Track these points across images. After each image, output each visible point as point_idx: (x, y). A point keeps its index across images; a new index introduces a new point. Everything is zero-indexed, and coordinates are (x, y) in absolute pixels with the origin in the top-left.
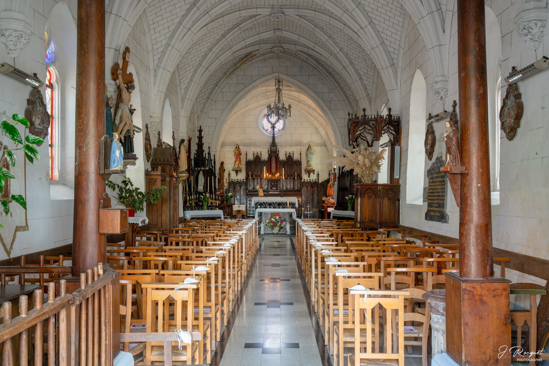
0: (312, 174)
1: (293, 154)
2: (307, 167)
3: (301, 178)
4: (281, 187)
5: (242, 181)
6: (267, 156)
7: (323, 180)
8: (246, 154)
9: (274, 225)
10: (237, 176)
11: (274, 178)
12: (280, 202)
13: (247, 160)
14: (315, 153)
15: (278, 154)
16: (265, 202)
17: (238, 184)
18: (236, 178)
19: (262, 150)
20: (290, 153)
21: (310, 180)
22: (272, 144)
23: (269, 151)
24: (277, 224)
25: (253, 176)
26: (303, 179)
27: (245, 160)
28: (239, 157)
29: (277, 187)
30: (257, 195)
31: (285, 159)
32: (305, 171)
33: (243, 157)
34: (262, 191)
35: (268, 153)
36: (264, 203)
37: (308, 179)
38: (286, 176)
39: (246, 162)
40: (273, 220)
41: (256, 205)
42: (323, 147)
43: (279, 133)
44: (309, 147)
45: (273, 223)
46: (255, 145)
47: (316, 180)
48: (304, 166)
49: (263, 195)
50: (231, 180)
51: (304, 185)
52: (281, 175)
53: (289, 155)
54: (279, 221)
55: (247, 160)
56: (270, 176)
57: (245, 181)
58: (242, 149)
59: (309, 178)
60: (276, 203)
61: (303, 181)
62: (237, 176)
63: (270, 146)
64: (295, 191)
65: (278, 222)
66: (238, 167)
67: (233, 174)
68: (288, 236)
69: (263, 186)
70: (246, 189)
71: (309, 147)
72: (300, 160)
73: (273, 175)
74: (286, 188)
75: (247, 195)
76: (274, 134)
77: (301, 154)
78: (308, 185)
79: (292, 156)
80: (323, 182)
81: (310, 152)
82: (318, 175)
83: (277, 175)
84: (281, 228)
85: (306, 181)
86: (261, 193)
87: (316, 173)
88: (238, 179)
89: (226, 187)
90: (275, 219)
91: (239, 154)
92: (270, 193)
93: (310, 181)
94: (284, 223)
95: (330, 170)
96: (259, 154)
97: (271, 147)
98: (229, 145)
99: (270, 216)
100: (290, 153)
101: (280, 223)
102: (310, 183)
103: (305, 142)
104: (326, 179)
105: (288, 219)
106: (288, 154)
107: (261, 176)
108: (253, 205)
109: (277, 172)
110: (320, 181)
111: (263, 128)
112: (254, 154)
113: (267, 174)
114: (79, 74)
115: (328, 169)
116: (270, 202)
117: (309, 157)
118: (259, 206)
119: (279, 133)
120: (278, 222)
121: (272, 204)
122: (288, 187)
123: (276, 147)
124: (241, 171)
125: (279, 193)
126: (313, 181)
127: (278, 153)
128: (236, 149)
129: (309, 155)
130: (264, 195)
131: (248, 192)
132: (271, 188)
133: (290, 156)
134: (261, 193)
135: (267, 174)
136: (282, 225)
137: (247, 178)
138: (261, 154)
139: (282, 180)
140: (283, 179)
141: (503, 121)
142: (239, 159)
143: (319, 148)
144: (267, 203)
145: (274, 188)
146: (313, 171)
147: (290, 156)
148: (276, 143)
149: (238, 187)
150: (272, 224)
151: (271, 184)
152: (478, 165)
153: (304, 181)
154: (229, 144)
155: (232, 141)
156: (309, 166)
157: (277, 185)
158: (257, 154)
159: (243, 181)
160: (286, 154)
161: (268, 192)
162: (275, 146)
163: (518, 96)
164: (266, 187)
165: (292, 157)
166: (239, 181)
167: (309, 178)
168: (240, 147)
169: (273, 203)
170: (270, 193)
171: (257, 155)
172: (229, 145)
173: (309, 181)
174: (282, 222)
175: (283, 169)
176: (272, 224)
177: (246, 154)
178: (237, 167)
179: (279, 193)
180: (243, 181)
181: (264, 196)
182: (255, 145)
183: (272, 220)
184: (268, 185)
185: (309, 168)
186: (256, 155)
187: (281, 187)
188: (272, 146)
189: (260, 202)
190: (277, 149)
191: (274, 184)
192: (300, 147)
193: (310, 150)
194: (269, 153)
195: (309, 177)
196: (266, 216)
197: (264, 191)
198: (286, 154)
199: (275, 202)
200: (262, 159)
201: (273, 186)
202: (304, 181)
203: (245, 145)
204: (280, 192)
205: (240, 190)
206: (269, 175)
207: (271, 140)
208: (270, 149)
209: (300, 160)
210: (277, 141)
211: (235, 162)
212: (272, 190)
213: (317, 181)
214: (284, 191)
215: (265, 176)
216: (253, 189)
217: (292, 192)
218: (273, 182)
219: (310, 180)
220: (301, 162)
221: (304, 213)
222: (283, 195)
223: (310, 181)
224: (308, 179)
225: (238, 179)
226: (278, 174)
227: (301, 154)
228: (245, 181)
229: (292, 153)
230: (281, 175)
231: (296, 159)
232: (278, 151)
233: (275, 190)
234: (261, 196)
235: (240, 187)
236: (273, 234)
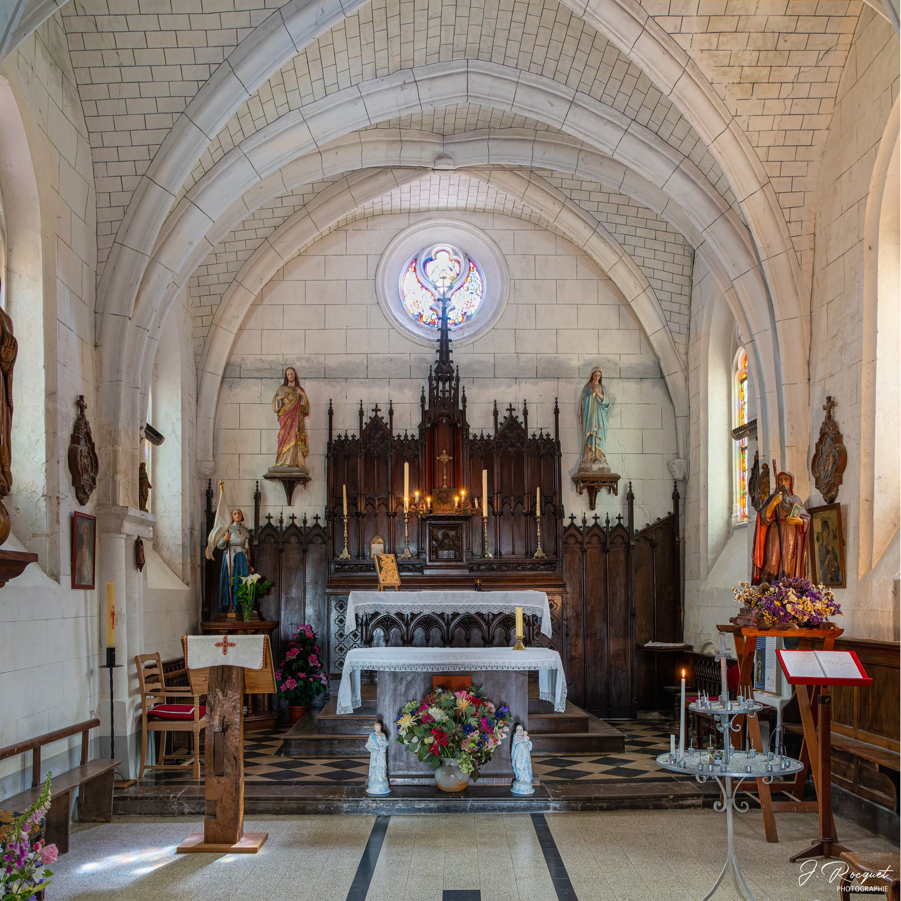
0: (603, 495)
1: (526, 413)
2: (588, 465)
3: (558, 512)
4: (477, 550)
5: (310, 523)
6: (417, 419)
7: (652, 521)
8: (331, 413)
9: (444, 744)
10: (290, 503)
11: (443, 510)
12: (473, 612)
13: (335, 438)
14: (616, 410)
15: (463, 413)
16: (407, 612)
17: (293, 540)
18: (288, 511)
19: (396, 397)
20: (511, 410)
21: (596, 518)
22: (436, 371)
23: (423, 399)
24: (459, 743)
25: (355, 505)
26: (567, 514)
27: (325, 439)
28: (296, 424)
29: (456, 547)
30: (372, 584)
31: (492, 433)
32: (576, 480)
33: (315, 424)
34: (394, 565)
35: (423, 406)
36: (400, 615)
37: (590, 514)
38: (497, 502)
39: (329, 444)
40: (436, 713)
41: (367, 624)
42: (647, 384)
43: (468, 326)
44: (594, 380)
45: (440, 735)
46: (368, 376)
47: (619, 518)
48: (570, 463)
49: (398, 583)
50: (263, 522)
51: (572, 541)
52: (475, 494)
53: (507, 414)
54: (473, 722)
55: (335, 438)
56: (429, 500)
57: (322, 523)
58: (309, 387)
59: (593, 513)
60: (455, 615)
61: (566, 522)
62: (290, 503)
63: (430, 379)
64: (535, 566)
65: (468, 729)
66: (295, 463)
67: (274, 494)
68: (523, 804)
69: (401, 545)
70: (330, 556)
71: (594, 380)
72: (552, 436)
73: (443, 498)
74: (497, 553)
75: (331, 583)
76: (444, 331)
77: (557, 412)
78: (587, 539)
79: (521, 419)
80: (649, 529)
81: (599, 402)
82: (630, 497)
83: (457, 499)
84: (481, 757)
85: (578, 523)
86: (389, 573)
87: (621, 485)
88: (293, 517)
89: (239, 550)
90: (450, 708)
91: (295, 409)
92: (427, 572)
93: (596, 525)
94: (501, 734)
95: (679, 476)
96: (384, 414)
97: (434, 382)
98: (259, 375)
99: (418, 690)
100: (511, 410)
101: (476, 736)
102: (596, 531)
103: (575, 362)
104: (663, 515)
105: (518, 707)
106: (503, 413)
107: (393, 505)
108: (350, 625)
109: (455, 486)
110: (639, 524)
111: (404, 312)
112: (361, 413)
113: (417, 494)
114: (895, 886)
115: (672, 473)
116: (427, 612)
117: (594, 422)
118: (379, 632)
119: (468, 326)
120: (468, 729)
121: (436, 622)
122: (506, 549)
123: (453, 383)
124: (305, 480)
125: (466, 572)
126: (608, 521)
127: (461, 407)
128: (287, 389)
129: (596, 415)
130: (402, 581)
131: (337, 570)
132: (434, 551)
133: (512, 421)
134: (389, 573)
135: (417, 494)
136: (491, 746)
137: (333, 512)
138: (391, 413)
139: (477, 520)
140: (485, 514)
141: (753, 495)
142: (295, 431)
143: (631, 387)
144: (414, 616)
145: (444, 554)
146: (611, 482)
147: (512, 421)
148: (454, 366)
149: (292, 555)
150: (429, 740)
151: (433, 537)
152: (846, 532)
153: (572, 524)
154: (258, 370)
155: (270, 358)
156: (595, 460)
157: (459, 538)
158: (376, 410)
159: (317, 526)
160: (496, 413)
161: (421, 570)
162: (450, 379)
163: (838, 438)
164: (413, 548)
165: (519, 425)
166: (299, 523)
167: (593, 513)
168: (307, 385)
169: (442, 615)
170: (427, 572)
171: (373, 414)
172: (259, 375)
173: (591, 523)
174: (486, 729)
175: (485, 473)
176: (429, 740)
177: (331, 413)
178: (288, 462)
179: (466, 572)
180: (317, 526)
181: (400, 588)
182: (368, 376)
183: (429, 717)
184: (420, 541)
185: (595, 467)
186: (369, 414)
187: (477, 550)
188: (438, 379)
189: (383, 613)
190: (456, 390)
191: (446, 536)
192: (554, 383)
193: (598, 390)
194: (427, 408)
195: (592, 506)
196: (402, 688)
197: (401, 567)
198: (496, 413)
199: (449, 612)
200: (395, 433)
201: (442, 546)
202: (572, 524)
203: (326, 375)
204: (471, 570)
205: (303, 562)
206: (422, 498)
207: (432, 356)
208: (431, 390)
209: (552, 436)
210: (457, 357)
211: (282, 443)
212: (437, 560)
213: (625, 523)
214: (489, 565)
215: (406, 499)
216: (358, 557)
217: (524, 569)
218: (441, 527)
219: (596, 518)
220: (558, 443)
221: (687, 709)
222: (484, 581)
223: (596, 525)
224: (590, 514)
225: (293, 517)
226: (463, 493)
227: (557, 412)
228: (322, 523)
229: (521, 407)
230: (475, 494)
231: (538, 433)
232: (464, 400)
233: (448, 560)
234: (386, 588)
235: (305, 551)
236: (435, 792)
